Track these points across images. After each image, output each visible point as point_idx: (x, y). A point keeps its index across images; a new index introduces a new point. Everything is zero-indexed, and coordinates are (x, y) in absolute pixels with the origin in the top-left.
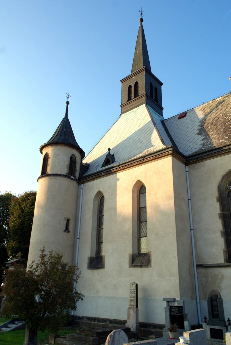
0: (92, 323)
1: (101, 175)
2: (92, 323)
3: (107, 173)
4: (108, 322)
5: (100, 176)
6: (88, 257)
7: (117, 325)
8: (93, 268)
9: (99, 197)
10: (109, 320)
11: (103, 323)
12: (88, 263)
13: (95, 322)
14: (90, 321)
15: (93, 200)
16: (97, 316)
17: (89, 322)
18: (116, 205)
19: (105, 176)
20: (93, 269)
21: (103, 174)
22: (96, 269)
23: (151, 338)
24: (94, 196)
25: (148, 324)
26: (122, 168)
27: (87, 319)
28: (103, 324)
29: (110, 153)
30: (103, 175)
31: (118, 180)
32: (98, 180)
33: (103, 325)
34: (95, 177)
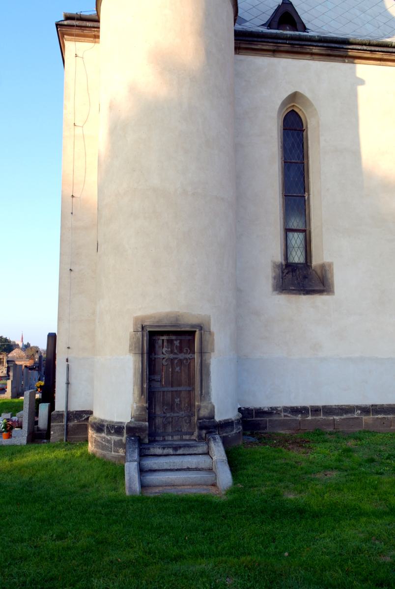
0: (310, 418)
1: (308, 51)
2: (310, 418)
3: (329, 52)
4: (359, 412)
5: (304, 51)
6: (274, 263)
7: (384, 416)
8: (294, 290)
9: (285, 109)
10: (358, 408)
11: (342, 415)
12: (274, 278)
13: (318, 415)
14: (300, 415)
15: (277, 113)
16: (320, 403)
17: (299, 417)
18: (358, 143)
19: (316, 57)
20: (295, 294)
21: (315, 50)
22: (304, 294)
23: (176, 445)
24: (280, 102)
25: (106, 424)
26: (378, 55)
27: (290, 413)
28: (342, 417)
29: (264, 23)
30: (312, 54)
31: (362, 82)
32: (290, 60)
33: (344, 419)
34: (287, 47)
